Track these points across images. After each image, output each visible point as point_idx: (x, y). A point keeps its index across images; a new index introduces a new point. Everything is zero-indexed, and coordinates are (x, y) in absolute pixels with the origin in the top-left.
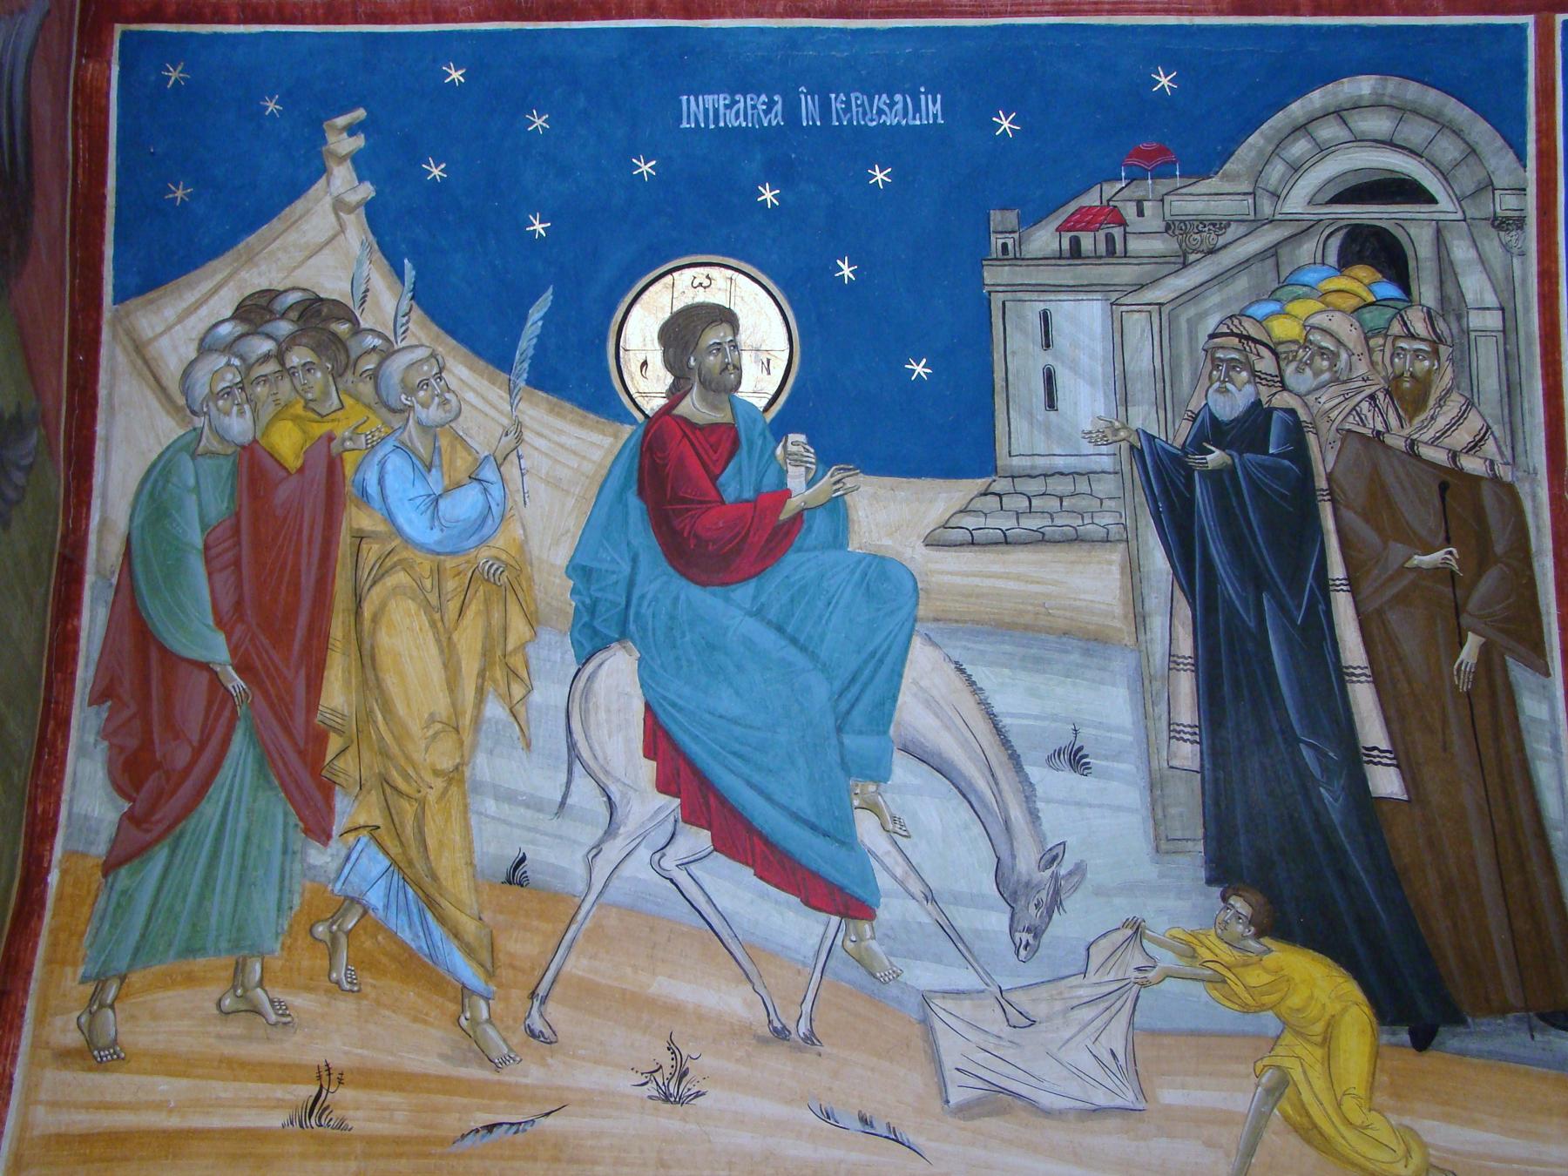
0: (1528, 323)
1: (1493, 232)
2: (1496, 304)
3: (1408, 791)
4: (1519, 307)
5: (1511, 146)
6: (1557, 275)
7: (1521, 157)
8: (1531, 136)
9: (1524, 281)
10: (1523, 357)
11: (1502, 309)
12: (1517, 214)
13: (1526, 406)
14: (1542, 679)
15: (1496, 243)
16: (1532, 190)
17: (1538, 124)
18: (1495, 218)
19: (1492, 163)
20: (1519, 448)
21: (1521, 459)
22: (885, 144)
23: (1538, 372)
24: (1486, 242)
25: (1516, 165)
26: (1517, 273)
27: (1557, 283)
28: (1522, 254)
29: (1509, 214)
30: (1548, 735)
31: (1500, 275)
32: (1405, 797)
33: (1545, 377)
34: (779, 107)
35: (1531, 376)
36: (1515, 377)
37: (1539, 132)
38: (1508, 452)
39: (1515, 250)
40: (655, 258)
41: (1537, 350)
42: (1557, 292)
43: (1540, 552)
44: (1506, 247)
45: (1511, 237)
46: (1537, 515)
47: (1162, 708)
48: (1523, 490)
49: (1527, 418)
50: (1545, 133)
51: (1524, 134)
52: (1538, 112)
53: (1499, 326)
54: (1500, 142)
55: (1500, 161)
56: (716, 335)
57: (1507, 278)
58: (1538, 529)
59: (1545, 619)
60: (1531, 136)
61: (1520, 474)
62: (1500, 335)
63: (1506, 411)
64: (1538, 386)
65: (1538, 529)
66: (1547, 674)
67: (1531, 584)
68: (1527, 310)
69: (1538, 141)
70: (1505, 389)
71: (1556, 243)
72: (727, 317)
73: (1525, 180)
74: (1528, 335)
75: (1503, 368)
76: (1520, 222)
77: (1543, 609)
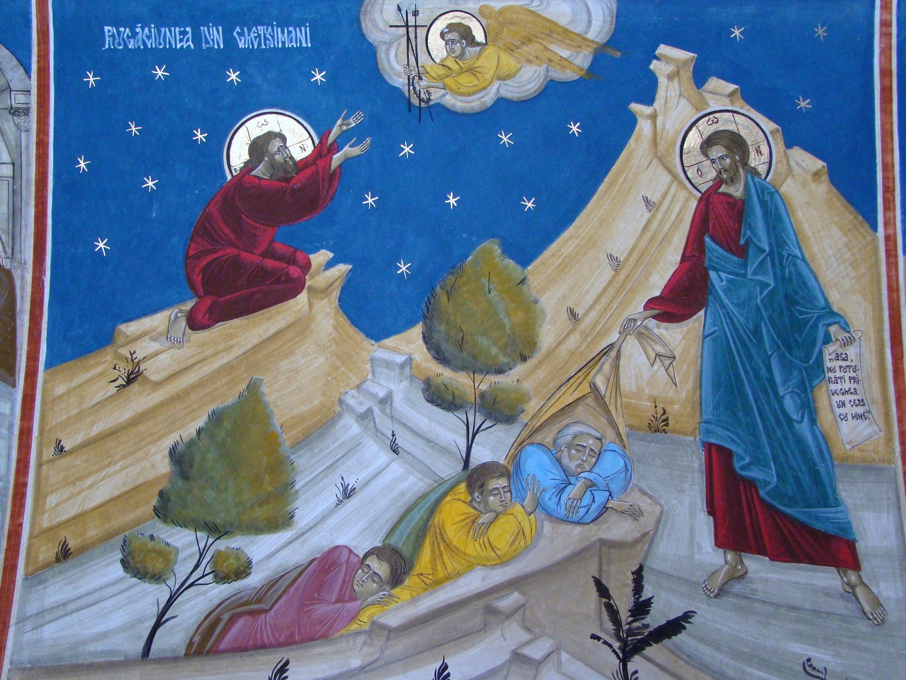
0: (28, 172)
1: (10, 116)
2: (9, 161)
3: (410, 324)
4: (24, 163)
5: (22, 65)
6: (48, 144)
7: (28, 71)
8: (34, 59)
9: (28, 147)
10: (24, 193)
11: (13, 164)
12: (25, 106)
13: (23, 222)
14: (10, 389)
15: (12, 124)
16: (34, 91)
17: (39, 51)
18: (12, 108)
19: (10, 75)
20: (17, 248)
21: (17, 255)
22: (167, 56)
23: (33, 202)
24: (5, 123)
25: (24, 76)
26: (24, 142)
27: (48, 148)
28: (27, 131)
29: (20, 106)
30: (7, 423)
31: (13, 143)
32: (421, 323)
33: (37, 206)
34: (190, 35)
35: (27, 204)
36: (18, 205)
37: (39, 56)
38: (9, 251)
39: (23, 128)
40: (281, 105)
41: (33, 189)
42: (47, 154)
43: (22, 311)
44: (18, 126)
45: (21, 120)
46: (23, 289)
47: (654, 225)
48: (17, 274)
49: (23, 231)
50: (43, 57)
51: (30, 57)
52: (39, 45)
53: (10, 173)
54: (15, 62)
55: (15, 75)
56: (276, 144)
57: (17, 145)
58: (22, 297)
59: (18, 352)
60: (34, 59)
61: (15, 264)
62: (11, 180)
63: (11, 226)
64: (32, 211)
65: (22, 297)
66: (14, 386)
67: (14, 331)
68: (28, 165)
69: (38, 62)
70: (11, 212)
71: (48, 125)
72: (270, 136)
73: (30, 86)
74: (28, 180)
75: (11, 200)
76: (26, 111)
77: (18, 346)
